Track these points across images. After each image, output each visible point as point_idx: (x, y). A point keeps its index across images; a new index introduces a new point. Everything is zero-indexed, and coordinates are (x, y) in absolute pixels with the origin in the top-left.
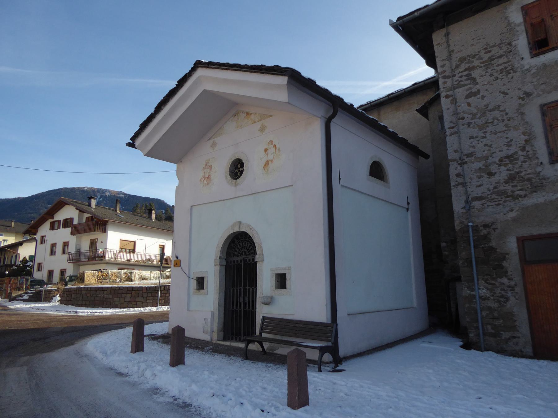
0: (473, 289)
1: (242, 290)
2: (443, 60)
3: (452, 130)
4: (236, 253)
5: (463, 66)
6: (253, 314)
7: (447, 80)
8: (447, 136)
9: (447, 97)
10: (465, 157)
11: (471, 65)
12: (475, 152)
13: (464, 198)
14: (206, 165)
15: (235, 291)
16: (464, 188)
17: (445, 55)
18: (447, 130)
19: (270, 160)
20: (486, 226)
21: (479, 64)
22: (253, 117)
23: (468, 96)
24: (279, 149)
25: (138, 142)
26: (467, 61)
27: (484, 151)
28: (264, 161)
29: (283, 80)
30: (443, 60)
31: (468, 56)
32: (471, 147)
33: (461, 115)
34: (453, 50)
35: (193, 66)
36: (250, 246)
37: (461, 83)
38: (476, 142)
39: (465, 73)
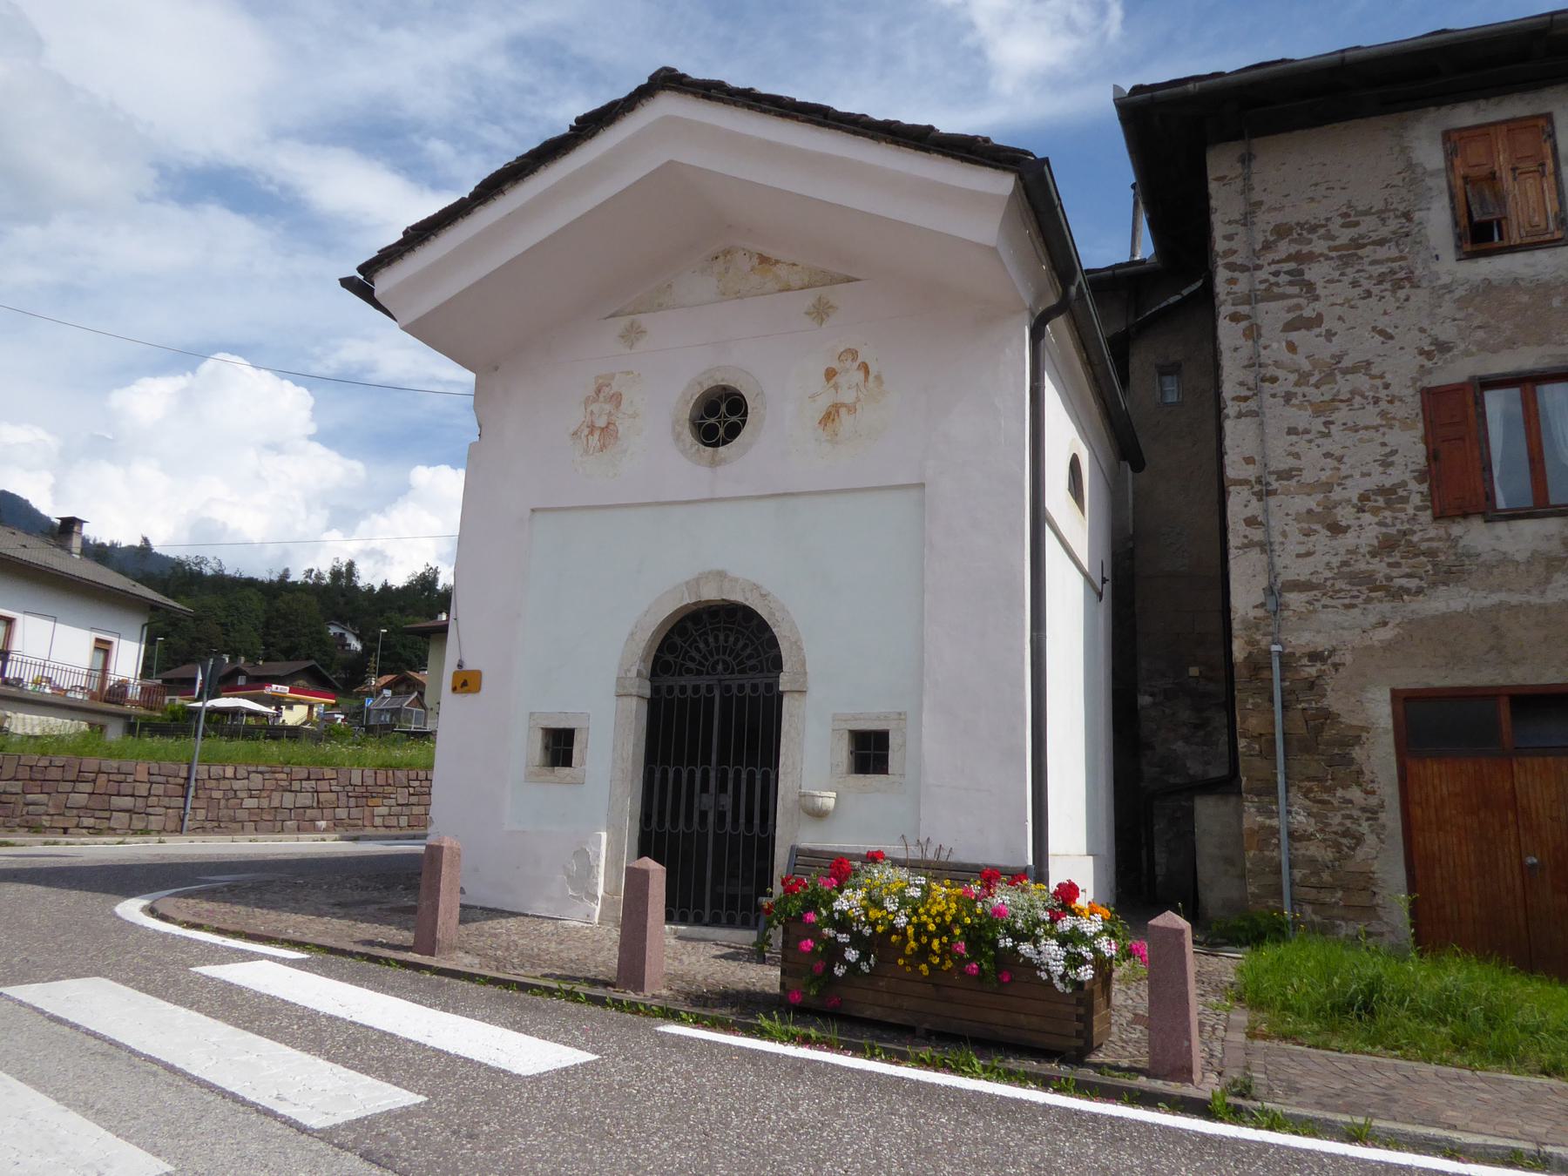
1: (712, 774)
2: (1230, 222)
3: (1243, 405)
5: (1284, 248)
7: (1236, 274)
8: (1227, 416)
9: (1235, 318)
10: (1272, 479)
11: (1305, 249)
13: (1263, 582)
14: (599, 391)
15: (671, 775)
18: (1229, 403)
19: (843, 405)
20: (1315, 657)
22: (782, 271)
23: (1290, 327)
24: (878, 378)
25: (384, 284)
28: (824, 402)
29: (1003, 184)
30: (1230, 222)
33: (1270, 371)
34: (1261, 203)
35: (645, 81)
36: (745, 646)
37: (1275, 290)
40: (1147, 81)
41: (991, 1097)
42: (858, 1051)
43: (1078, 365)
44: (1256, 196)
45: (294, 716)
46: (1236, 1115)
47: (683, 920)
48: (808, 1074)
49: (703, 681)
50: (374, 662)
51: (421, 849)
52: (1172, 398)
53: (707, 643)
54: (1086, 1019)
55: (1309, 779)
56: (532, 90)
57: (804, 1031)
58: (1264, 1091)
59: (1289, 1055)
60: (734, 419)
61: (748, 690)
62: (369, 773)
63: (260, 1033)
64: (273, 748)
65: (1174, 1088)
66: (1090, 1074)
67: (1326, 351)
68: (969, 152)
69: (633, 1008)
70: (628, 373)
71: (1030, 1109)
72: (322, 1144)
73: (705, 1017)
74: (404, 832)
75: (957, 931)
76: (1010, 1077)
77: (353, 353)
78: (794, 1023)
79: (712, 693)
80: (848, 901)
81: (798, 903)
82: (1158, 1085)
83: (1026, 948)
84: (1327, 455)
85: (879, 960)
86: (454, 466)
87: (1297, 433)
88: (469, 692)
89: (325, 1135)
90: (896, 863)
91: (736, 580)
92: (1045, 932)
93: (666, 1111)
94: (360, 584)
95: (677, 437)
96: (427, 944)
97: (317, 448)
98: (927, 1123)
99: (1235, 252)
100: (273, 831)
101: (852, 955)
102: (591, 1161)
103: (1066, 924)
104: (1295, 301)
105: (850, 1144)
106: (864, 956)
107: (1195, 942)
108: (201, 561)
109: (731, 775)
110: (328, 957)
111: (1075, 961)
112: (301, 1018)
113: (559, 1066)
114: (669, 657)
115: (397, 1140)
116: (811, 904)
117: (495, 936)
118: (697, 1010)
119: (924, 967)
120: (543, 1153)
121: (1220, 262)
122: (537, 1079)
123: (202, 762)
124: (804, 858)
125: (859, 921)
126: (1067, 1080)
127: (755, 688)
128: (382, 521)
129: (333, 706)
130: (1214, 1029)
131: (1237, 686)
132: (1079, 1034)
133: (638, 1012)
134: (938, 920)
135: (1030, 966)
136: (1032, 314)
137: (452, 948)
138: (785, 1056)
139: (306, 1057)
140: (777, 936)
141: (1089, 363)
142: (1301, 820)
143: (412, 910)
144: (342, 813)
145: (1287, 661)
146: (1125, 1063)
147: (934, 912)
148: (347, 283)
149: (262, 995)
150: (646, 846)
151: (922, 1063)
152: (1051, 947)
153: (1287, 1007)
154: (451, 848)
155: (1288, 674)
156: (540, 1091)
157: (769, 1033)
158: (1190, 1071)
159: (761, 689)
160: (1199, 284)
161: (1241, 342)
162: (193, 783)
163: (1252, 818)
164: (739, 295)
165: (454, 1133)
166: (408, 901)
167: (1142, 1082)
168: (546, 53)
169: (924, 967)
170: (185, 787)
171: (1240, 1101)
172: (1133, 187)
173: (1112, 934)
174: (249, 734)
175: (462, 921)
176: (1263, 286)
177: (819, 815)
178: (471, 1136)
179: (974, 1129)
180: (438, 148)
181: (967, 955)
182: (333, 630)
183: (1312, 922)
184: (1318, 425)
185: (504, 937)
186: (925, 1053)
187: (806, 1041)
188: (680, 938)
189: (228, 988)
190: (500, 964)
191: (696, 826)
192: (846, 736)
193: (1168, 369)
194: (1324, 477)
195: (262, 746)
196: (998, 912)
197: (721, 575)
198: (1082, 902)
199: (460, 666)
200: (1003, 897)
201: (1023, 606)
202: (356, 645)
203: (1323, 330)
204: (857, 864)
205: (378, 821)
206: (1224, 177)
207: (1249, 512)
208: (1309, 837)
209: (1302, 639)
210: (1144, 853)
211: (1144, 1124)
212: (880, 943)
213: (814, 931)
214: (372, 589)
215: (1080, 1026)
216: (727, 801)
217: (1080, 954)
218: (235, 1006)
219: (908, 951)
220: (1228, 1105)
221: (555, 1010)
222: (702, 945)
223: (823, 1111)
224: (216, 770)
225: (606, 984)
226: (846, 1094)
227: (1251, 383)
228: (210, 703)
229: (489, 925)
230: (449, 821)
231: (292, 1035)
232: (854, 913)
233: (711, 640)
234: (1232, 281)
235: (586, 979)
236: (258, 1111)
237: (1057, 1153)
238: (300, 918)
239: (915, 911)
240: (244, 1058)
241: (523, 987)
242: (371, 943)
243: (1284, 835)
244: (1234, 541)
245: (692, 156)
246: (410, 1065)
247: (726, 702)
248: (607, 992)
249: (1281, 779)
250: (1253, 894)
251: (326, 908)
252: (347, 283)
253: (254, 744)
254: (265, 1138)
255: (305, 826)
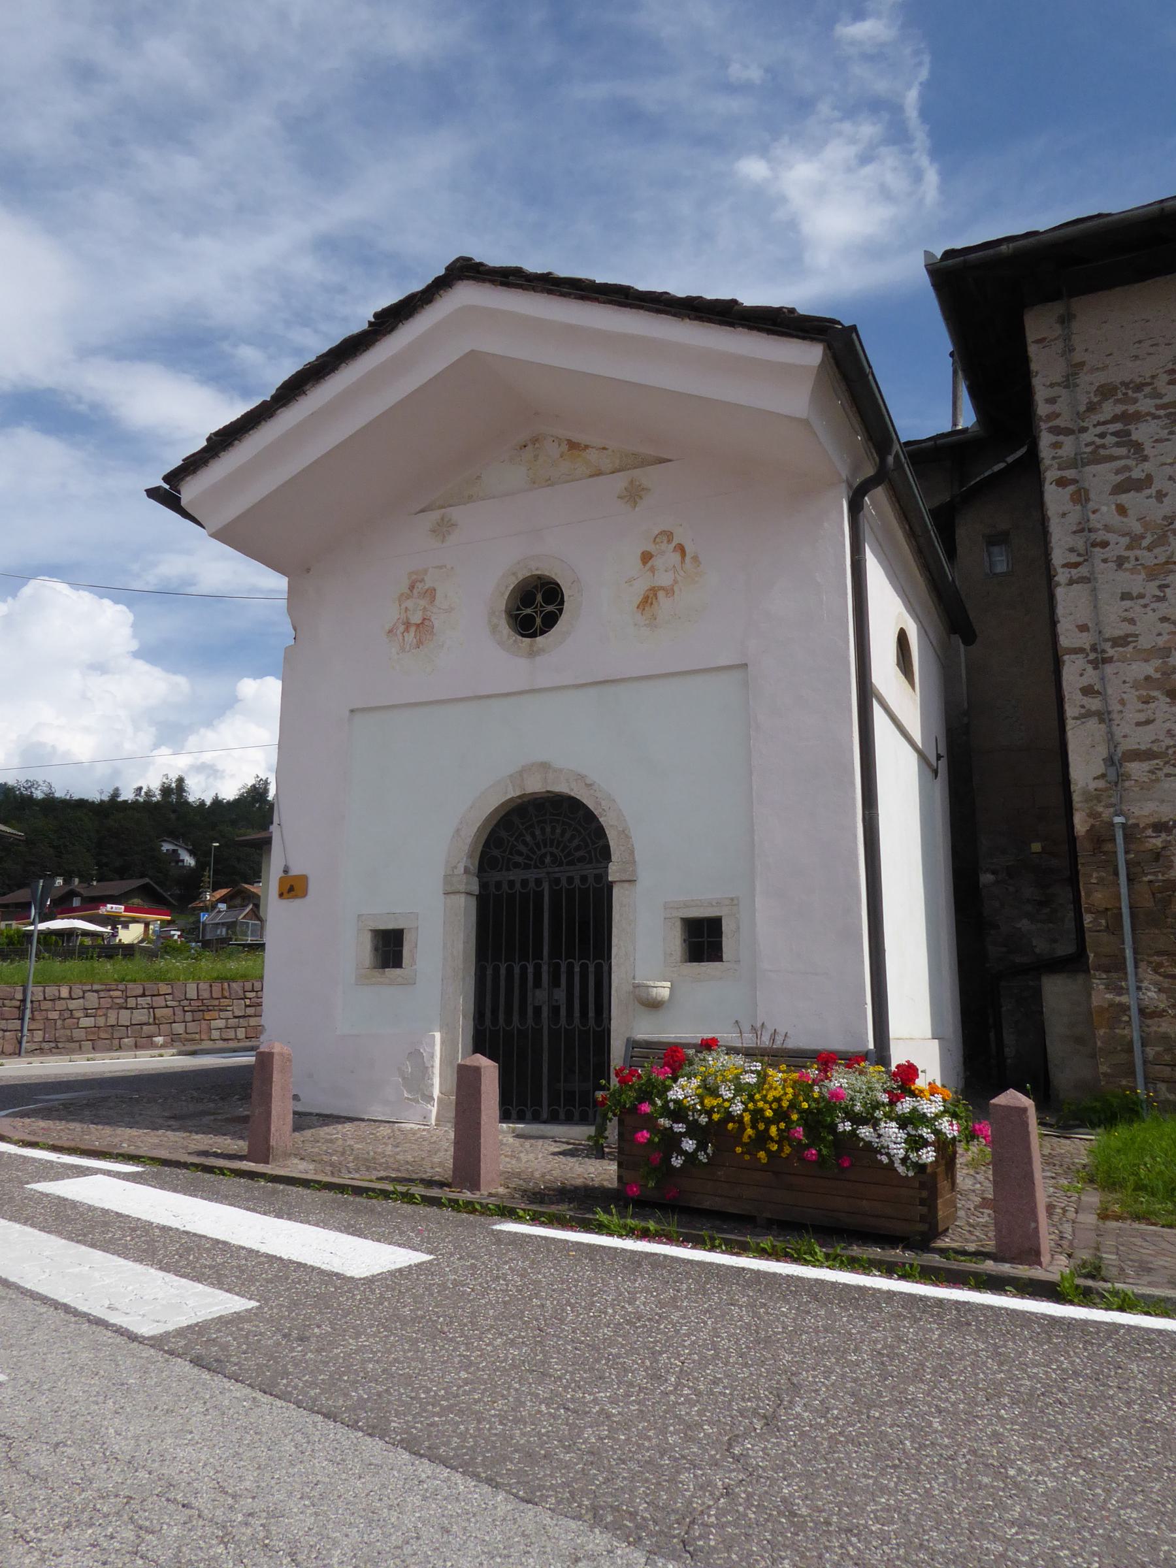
0: (1122, 988)
1: (545, 968)
2: (1052, 385)
3: (1074, 571)
4: (519, 859)
5: (1109, 409)
6: (603, 1037)
7: (1061, 438)
8: (1058, 584)
9: (1061, 483)
10: (1107, 646)
11: (1131, 409)
12: (1137, 636)
13: (1102, 751)
14: (412, 587)
15: (503, 971)
16: (1103, 726)
17: (1058, 372)
18: (1060, 570)
19: (662, 588)
20: (1160, 827)
21: (1153, 410)
22: (593, 456)
23: (1119, 489)
24: (695, 559)
25: (189, 492)
26: (1120, 396)
27: (1160, 634)
28: (641, 587)
29: (811, 354)
30: (1052, 385)
31: (1123, 383)
32: (1125, 620)
33: (1101, 536)
34: (1082, 364)
35: (442, 272)
36: (573, 837)
37: (1102, 452)
38: (1138, 609)
39: (1113, 427)
40: (959, 245)
41: (834, 1285)
42: (698, 1242)
43: (900, 535)
44: (1077, 357)
45: (130, 934)
46: (1086, 1297)
47: (521, 1118)
48: (646, 1267)
49: (531, 875)
50: (208, 876)
51: (248, 1059)
52: (1001, 568)
53: (533, 836)
54: (930, 1203)
55: (1160, 953)
56: (342, 289)
57: (643, 1224)
58: (1115, 1271)
59: (1143, 1236)
60: (550, 608)
61: (577, 881)
62: (204, 986)
63: (93, 1245)
64: (107, 967)
65: (1023, 1271)
66: (936, 1260)
67: (1158, 512)
68: (774, 324)
69: (469, 1207)
70: (441, 567)
71: (873, 1295)
72: (152, 1351)
73: (542, 1214)
74: (241, 1044)
75: (795, 1117)
76: (853, 1264)
77: (171, 567)
78: (633, 1217)
79: (541, 886)
80: (683, 1090)
81: (633, 1094)
82: (1006, 1268)
83: (865, 1132)
84: (1164, 619)
85: (717, 1149)
86: (278, 678)
87: (1132, 599)
88: (296, 897)
89: (157, 1342)
90: (731, 1050)
91: (561, 770)
92: (885, 1114)
93: (500, 1308)
94: (191, 799)
95: (494, 629)
96: (261, 1152)
97: (141, 666)
98: (767, 1313)
99: (1058, 415)
100: (110, 1049)
101: (689, 1145)
102: (422, 1360)
103: (906, 1106)
104: (1122, 462)
105: (688, 1335)
106: (701, 1146)
107: (1042, 1124)
108: (32, 785)
109: (563, 969)
110: (163, 1170)
111: (916, 1143)
112: (134, 1230)
113: (393, 1267)
114: (496, 852)
115: (228, 1345)
116: (646, 1095)
117: (331, 1141)
118: (534, 1207)
119: (762, 1154)
120: (375, 1353)
121: (1043, 426)
122: (370, 1281)
123: (37, 983)
124: (639, 1049)
125: (694, 1110)
126: (911, 1265)
127: (584, 879)
128: (210, 736)
129: (169, 923)
130: (1064, 1210)
131: (1080, 860)
132: (923, 1219)
133: (474, 1211)
134: (775, 1106)
135: (871, 1150)
136: (850, 486)
137: (287, 1155)
138: (624, 1250)
139: (139, 1268)
140: (612, 1131)
141: (912, 534)
142: (1152, 996)
143: (245, 1119)
144: (179, 1028)
145: (1131, 833)
146: (971, 1247)
147: (770, 1097)
148: (153, 493)
149: (96, 1209)
150: (482, 1043)
151: (763, 1254)
152: (891, 1130)
153: (1139, 1187)
154: (282, 1054)
155: (1133, 847)
156: (373, 1291)
157: (608, 1228)
158: (1038, 1253)
159: (591, 880)
160: (1023, 450)
161: (1069, 506)
162: (29, 1005)
163: (1101, 996)
164: (550, 483)
165: (285, 1336)
166: (242, 1111)
167: (989, 1266)
168: (351, 250)
169: (762, 1154)
170: (21, 1009)
171: (1090, 1283)
172: (952, 355)
173: (954, 1115)
174: (84, 953)
175: (297, 1128)
176: (1089, 449)
177: (654, 1005)
178: (302, 1339)
179: (815, 1317)
180: (248, 354)
181: (805, 1141)
182: (166, 847)
183: (1168, 1100)
184: (1152, 588)
185: (340, 1142)
186: (766, 1243)
187: (645, 1235)
188: (518, 1136)
189: (62, 1202)
190: (336, 1169)
191: (530, 1022)
192: (678, 924)
193: (996, 539)
194: (1161, 641)
195: (96, 964)
196: (836, 1095)
197: (545, 766)
198: (921, 1083)
199: (286, 871)
200: (840, 1080)
201: (853, 784)
202: (189, 861)
203: (1152, 491)
204: (691, 1052)
205: (215, 1034)
206: (1044, 339)
207: (1084, 681)
208: (1159, 1014)
209: (1144, 810)
210: (992, 1035)
211: (991, 1308)
212: (717, 1132)
213: (649, 1122)
214: (203, 803)
215: (924, 1210)
216: (560, 995)
217: (921, 1136)
218: (69, 1221)
219: (745, 1139)
220: (1078, 1286)
221: (390, 1213)
222: (540, 1142)
223: (661, 1304)
224: (51, 991)
225: (442, 1185)
226: (685, 1286)
227: (1082, 550)
228: (42, 926)
229: (325, 1131)
230: (280, 1028)
231: (125, 1246)
232: (689, 1102)
233: (538, 832)
234: (1056, 445)
235: (422, 1181)
236: (89, 1321)
237: (900, 1340)
238: (134, 1132)
239: (751, 1098)
240: (77, 1270)
241: (358, 1191)
242: (205, 1154)
243: (1134, 1011)
244: (1071, 711)
245: (492, 344)
246: (242, 1272)
247: (555, 895)
248: (445, 1192)
249: (1129, 953)
250: (1105, 1074)
251: (160, 1121)
252: (153, 493)
253: (88, 964)
254: (96, 1347)
255: (143, 1043)
